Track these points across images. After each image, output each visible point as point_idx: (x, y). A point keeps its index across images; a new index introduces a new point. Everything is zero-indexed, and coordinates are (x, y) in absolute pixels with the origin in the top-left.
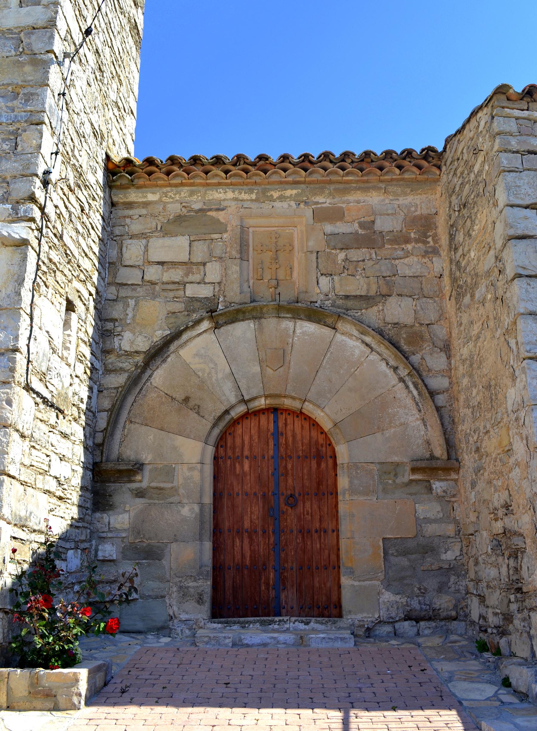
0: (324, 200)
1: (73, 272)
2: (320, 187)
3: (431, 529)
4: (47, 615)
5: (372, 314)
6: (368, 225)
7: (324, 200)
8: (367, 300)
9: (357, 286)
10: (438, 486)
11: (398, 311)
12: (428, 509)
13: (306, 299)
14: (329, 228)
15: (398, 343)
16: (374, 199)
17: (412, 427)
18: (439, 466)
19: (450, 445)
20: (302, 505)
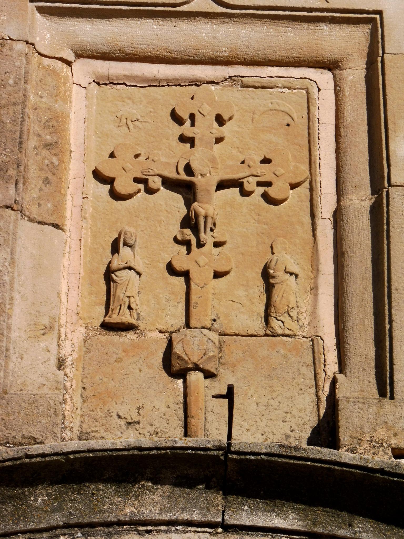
13: (381, 433)
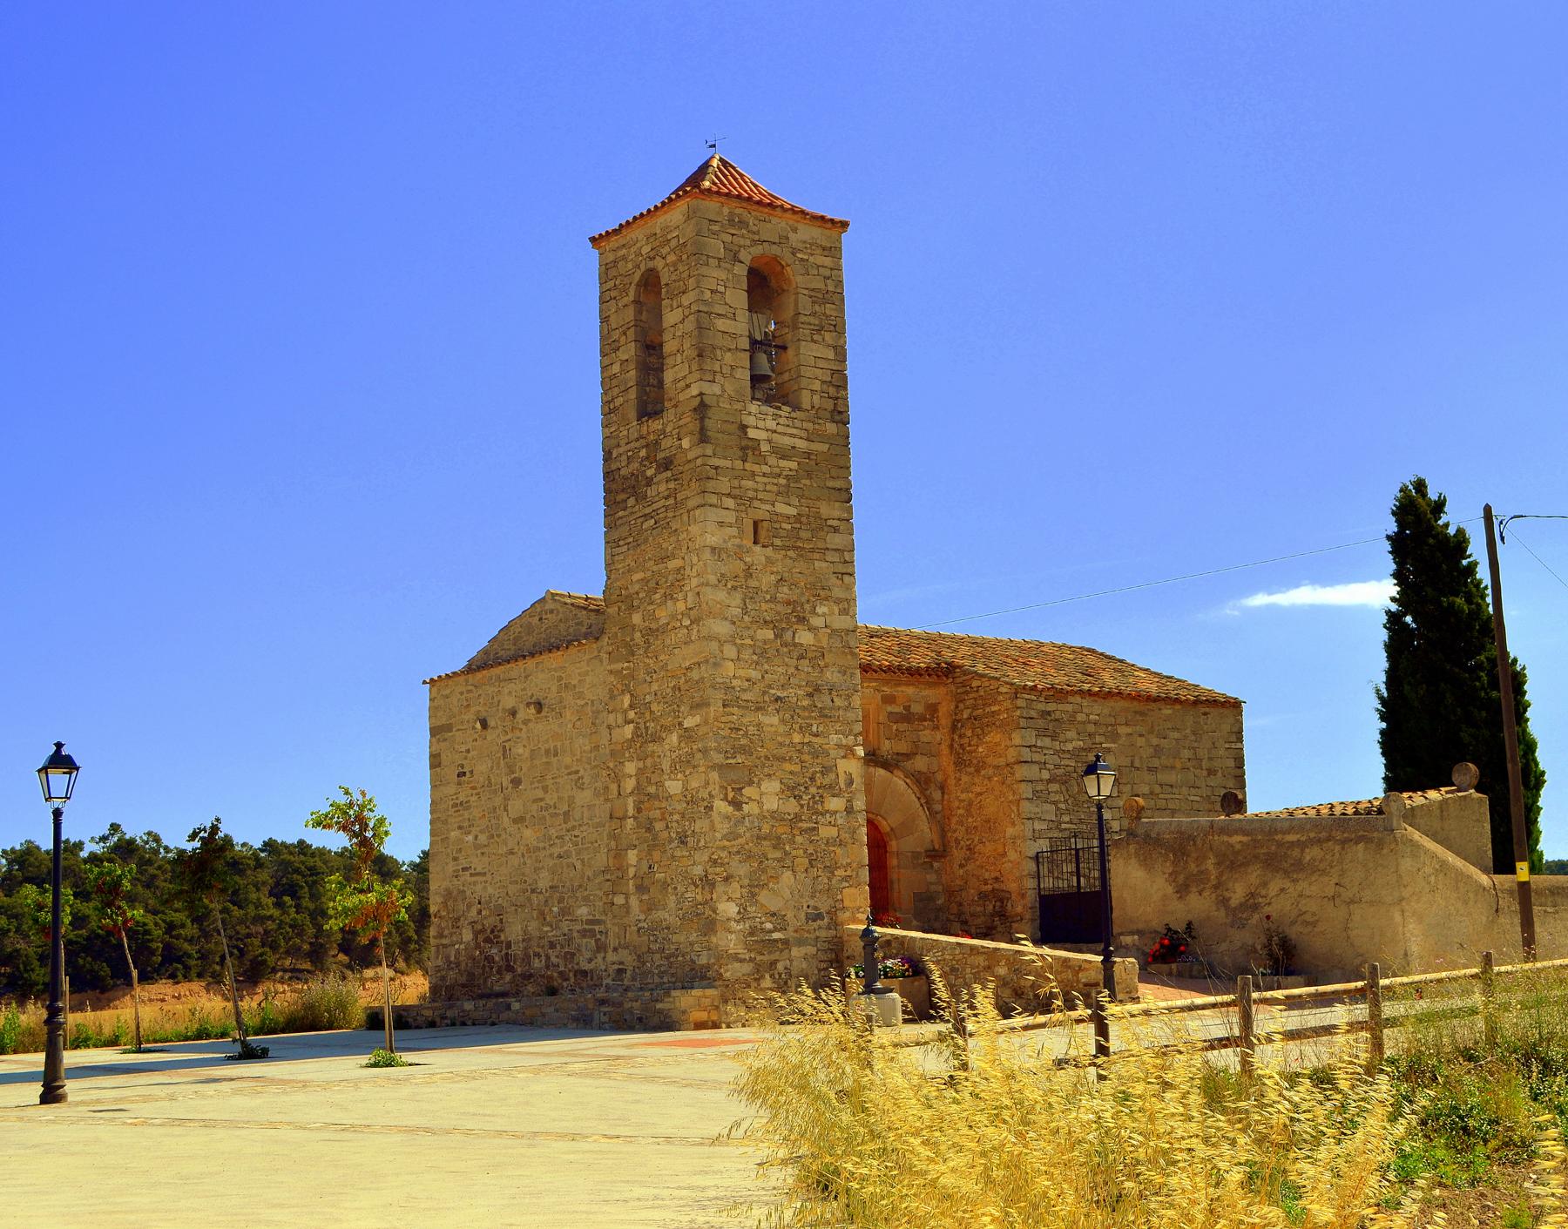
0: (887, 690)
1: (1044, 870)
2: (887, 682)
3: (933, 888)
4: (889, 963)
5: (908, 765)
6: (907, 708)
7: (887, 690)
8: (908, 756)
9: (903, 747)
10: (936, 865)
11: (920, 763)
12: (931, 877)
14: (889, 709)
15: (922, 782)
16: (910, 690)
17: (924, 833)
18: (936, 854)
19: (945, 845)
20: (1179, 1003)
